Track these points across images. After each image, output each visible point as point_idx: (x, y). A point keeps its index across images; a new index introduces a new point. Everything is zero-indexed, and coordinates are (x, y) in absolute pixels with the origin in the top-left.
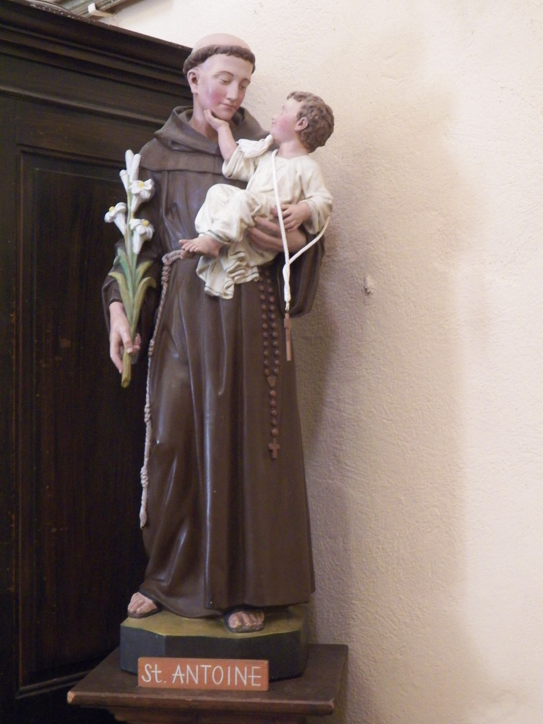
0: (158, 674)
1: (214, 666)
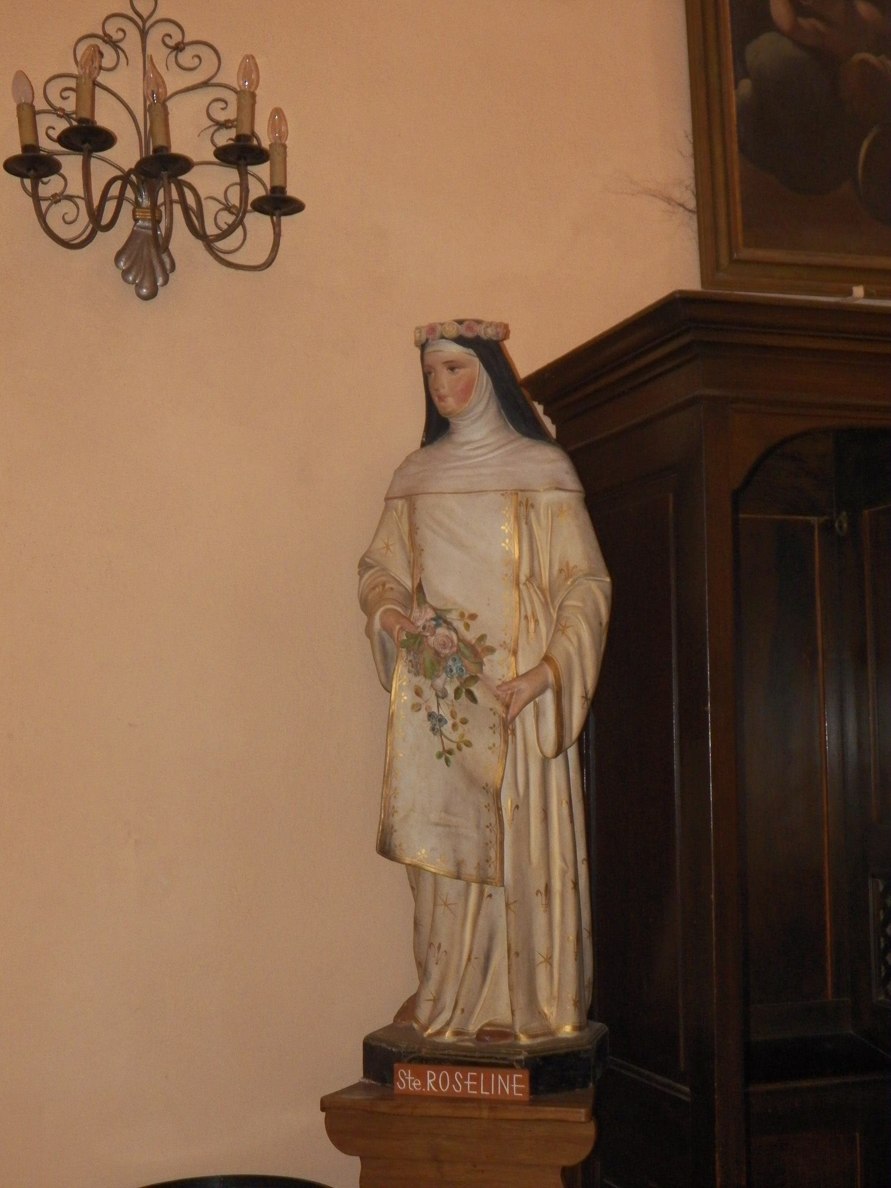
0: (467, 1081)
1: (415, 1079)
